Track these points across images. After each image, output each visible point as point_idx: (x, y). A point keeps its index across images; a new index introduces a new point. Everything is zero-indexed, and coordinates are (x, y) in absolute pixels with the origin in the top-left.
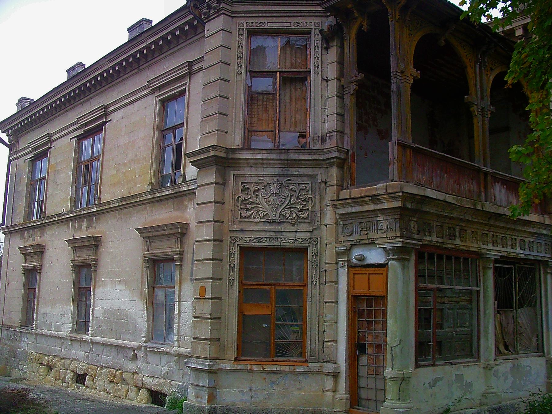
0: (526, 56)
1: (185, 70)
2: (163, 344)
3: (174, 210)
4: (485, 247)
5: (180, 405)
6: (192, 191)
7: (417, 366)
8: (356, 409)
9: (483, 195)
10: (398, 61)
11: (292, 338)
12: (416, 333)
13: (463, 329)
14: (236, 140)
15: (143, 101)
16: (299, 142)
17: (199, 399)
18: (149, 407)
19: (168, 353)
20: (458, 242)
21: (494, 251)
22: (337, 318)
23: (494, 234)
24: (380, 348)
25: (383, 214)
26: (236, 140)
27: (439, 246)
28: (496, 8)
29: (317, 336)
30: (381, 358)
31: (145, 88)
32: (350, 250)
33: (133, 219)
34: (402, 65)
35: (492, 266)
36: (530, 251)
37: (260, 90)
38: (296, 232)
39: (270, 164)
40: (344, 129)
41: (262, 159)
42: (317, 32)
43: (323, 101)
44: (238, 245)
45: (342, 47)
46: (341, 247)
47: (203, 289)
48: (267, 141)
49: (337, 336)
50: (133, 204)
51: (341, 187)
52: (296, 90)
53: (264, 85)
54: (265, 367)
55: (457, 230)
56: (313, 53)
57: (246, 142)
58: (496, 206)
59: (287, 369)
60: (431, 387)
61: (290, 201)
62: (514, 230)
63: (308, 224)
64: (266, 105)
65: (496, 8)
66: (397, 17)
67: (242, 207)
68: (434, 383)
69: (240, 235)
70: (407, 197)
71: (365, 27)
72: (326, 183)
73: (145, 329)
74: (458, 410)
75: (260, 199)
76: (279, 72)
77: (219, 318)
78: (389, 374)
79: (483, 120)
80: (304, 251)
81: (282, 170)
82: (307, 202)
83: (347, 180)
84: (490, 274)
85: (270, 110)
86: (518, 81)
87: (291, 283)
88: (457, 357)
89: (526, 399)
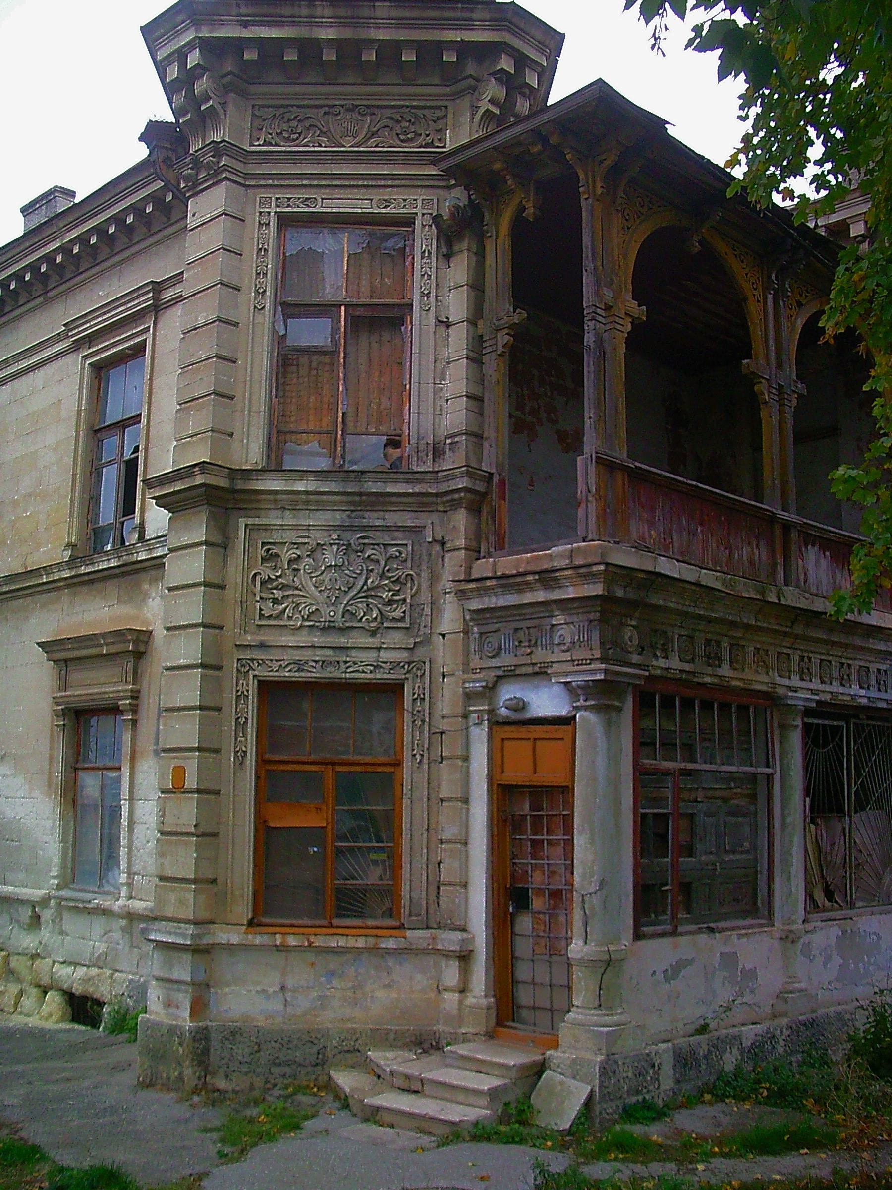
0: (862, 279)
1: (146, 301)
2: (95, 892)
3: (119, 602)
4: (786, 682)
5: (132, 1023)
6: (158, 562)
7: (638, 936)
8: (509, 1027)
9: (780, 570)
10: (598, 283)
11: (373, 877)
12: (636, 865)
13: (738, 857)
14: (250, 451)
15: (55, 365)
16: (385, 455)
17: (171, 1010)
18: (69, 1031)
19: (106, 912)
20: (725, 670)
21: (803, 690)
22: (467, 832)
23: (805, 655)
24: (559, 897)
25: (564, 611)
26: (250, 451)
27: (685, 680)
28: (802, 175)
29: (424, 872)
30: (562, 919)
31: (58, 338)
32: (495, 685)
33: (33, 621)
34: (608, 294)
35: (799, 722)
36: (879, 690)
37: (304, 343)
38: (379, 649)
39: (323, 503)
40: (481, 426)
41: (307, 493)
42: (428, 220)
43: (438, 371)
44: (255, 676)
45: (480, 255)
46: (474, 681)
47: (180, 772)
48: (319, 455)
49: (467, 871)
50: (33, 590)
51: (475, 552)
52: (380, 342)
53: (312, 333)
54: (312, 938)
55: (725, 644)
56: (417, 266)
57: (273, 456)
58: (807, 595)
59: (361, 943)
60: (667, 980)
61: (365, 583)
62: (846, 646)
63: (404, 631)
64: (317, 375)
65: (802, 175)
66: (599, 191)
67: (264, 595)
68: (674, 972)
69: (258, 655)
70: (616, 574)
71: (530, 212)
72: (443, 543)
73: (56, 860)
74: (726, 1028)
75: (303, 578)
76: (345, 305)
77: (215, 835)
78: (579, 952)
79: (781, 412)
80: (395, 689)
81: (349, 517)
82: (401, 583)
83: (487, 539)
84: (795, 739)
85: (326, 387)
86: (848, 328)
87: (367, 759)
88: (725, 917)
89: (868, 1002)
